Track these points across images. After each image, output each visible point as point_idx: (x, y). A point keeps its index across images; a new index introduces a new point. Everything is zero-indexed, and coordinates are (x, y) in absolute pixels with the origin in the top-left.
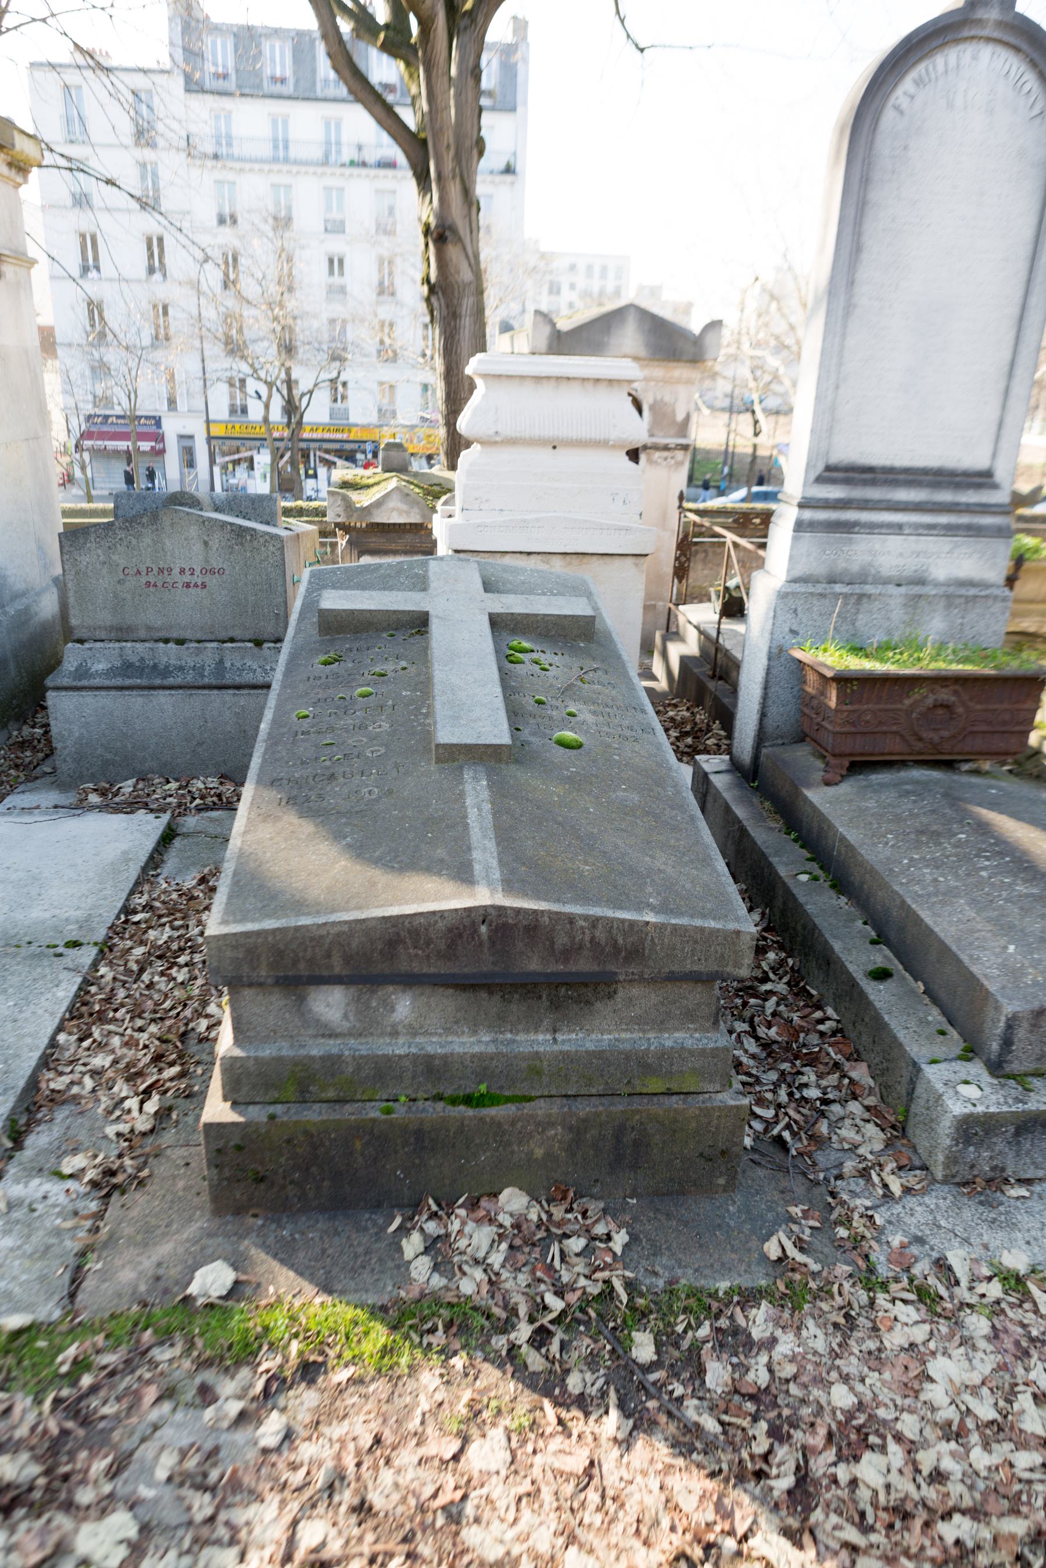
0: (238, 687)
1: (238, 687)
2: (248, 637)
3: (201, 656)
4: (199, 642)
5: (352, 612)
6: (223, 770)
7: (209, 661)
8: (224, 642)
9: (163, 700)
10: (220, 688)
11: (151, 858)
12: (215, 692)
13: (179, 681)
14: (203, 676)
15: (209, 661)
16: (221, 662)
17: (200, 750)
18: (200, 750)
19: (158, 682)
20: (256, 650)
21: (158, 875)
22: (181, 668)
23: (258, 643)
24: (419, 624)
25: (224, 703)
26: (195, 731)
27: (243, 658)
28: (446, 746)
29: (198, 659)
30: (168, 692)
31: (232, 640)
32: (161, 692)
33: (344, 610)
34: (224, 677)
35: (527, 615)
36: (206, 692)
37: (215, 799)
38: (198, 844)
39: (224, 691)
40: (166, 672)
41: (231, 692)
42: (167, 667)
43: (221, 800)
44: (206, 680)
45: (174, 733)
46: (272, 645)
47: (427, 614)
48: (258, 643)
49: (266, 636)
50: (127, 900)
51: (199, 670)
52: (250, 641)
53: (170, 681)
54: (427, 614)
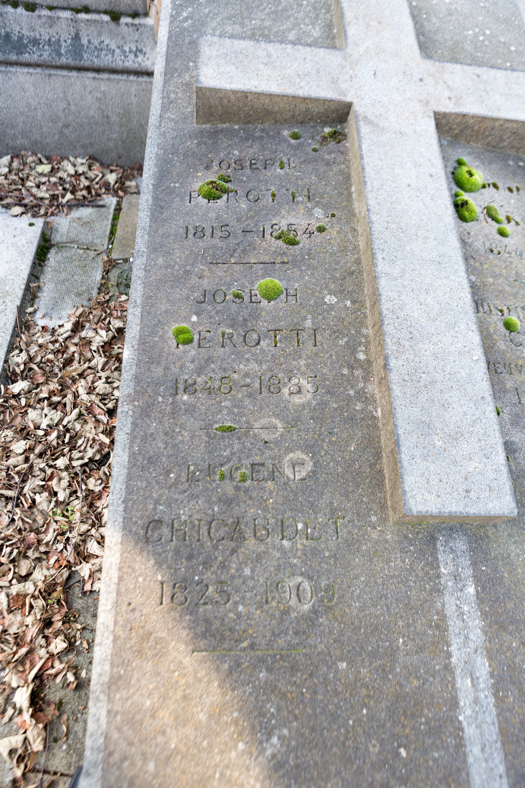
0: (98, 70)
1: (98, 70)
2: (103, 7)
3: (55, 28)
4: (51, 8)
5: (245, 95)
6: (90, 151)
7: (65, 36)
8: (78, 11)
9: (22, 78)
10: (80, 69)
11: (28, 288)
12: (74, 74)
13: (35, 58)
14: (59, 55)
15: (65, 36)
16: (77, 37)
17: (66, 131)
18: (66, 131)
19: (13, 57)
20: (113, 25)
21: (35, 311)
22: (35, 42)
23: (115, 17)
24: (335, 119)
25: (85, 87)
26: (60, 113)
27: (99, 34)
28: (421, 519)
29: (53, 31)
30: (26, 70)
31: (86, 10)
32: (19, 69)
33: (234, 92)
34: (81, 58)
35: (484, 119)
36: (65, 73)
37: (85, 193)
38: (71, 260)
39: (84, 74)
40: (20, 46)
41: (91, 75)
42: (20, 39)
43: (90, 192)
44: (64, 60)
45: (39, 113)
46: (129, 20)
47: (349, 106)
48: (115, 17)
49: (123, 8)
50: (6, 361)
51: (54, 45)
52: (106, 12)
53: (26, 57)
54: (349, 106)
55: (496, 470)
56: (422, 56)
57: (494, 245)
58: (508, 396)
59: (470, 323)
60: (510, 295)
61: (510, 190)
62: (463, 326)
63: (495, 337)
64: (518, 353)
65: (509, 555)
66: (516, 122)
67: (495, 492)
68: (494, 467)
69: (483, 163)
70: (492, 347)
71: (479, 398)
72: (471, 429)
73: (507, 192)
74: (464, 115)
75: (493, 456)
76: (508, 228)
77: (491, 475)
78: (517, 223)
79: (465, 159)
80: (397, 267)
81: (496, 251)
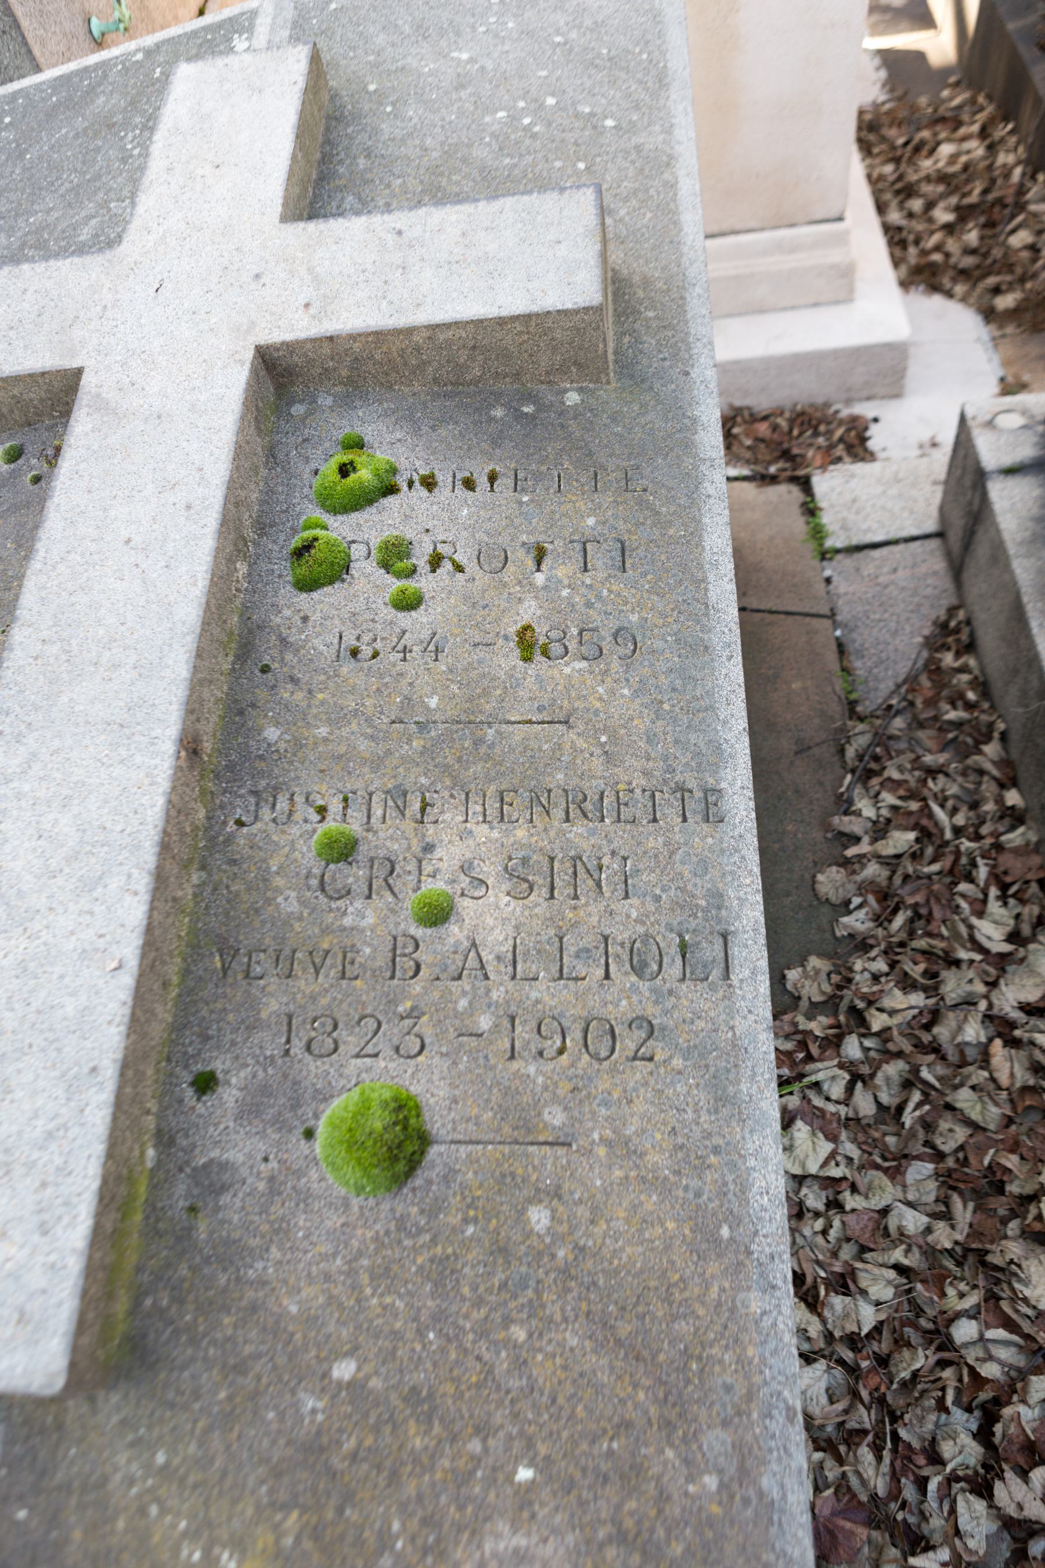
35: (379, 336)
55: (53, 1266)
56: (884, 85)
57: (366, 638)
58: (256, 1038)
59: (135, 872)
60: (364, 761)
61: (469, 484)
62: (115, 883)
63: (279, 882)
64: (330, 918)
65: (105, 1480)
66: (456, 324)
67: (30, 1328)
68: (53, 1257)
69: (417, 432)
70: (257, 911)
71: (86, 1070)
72: (35, 1155)
73: (460, 491)
74: (331, 338)
75: (59, 1231)
76: (425, 583)
77: (36, 1279)
78: (459, 568)
79: (368, 432)
80: (22, 749)
81: (366, 651)
